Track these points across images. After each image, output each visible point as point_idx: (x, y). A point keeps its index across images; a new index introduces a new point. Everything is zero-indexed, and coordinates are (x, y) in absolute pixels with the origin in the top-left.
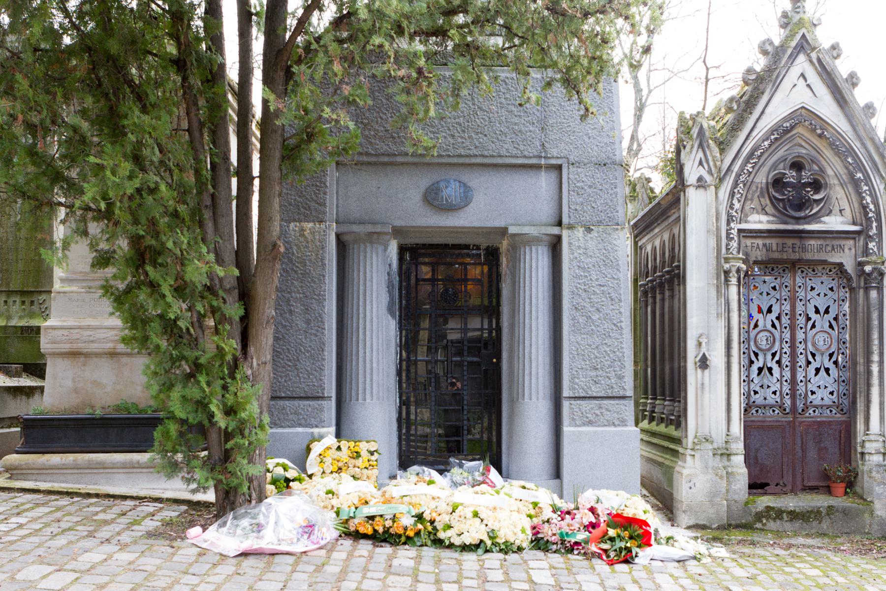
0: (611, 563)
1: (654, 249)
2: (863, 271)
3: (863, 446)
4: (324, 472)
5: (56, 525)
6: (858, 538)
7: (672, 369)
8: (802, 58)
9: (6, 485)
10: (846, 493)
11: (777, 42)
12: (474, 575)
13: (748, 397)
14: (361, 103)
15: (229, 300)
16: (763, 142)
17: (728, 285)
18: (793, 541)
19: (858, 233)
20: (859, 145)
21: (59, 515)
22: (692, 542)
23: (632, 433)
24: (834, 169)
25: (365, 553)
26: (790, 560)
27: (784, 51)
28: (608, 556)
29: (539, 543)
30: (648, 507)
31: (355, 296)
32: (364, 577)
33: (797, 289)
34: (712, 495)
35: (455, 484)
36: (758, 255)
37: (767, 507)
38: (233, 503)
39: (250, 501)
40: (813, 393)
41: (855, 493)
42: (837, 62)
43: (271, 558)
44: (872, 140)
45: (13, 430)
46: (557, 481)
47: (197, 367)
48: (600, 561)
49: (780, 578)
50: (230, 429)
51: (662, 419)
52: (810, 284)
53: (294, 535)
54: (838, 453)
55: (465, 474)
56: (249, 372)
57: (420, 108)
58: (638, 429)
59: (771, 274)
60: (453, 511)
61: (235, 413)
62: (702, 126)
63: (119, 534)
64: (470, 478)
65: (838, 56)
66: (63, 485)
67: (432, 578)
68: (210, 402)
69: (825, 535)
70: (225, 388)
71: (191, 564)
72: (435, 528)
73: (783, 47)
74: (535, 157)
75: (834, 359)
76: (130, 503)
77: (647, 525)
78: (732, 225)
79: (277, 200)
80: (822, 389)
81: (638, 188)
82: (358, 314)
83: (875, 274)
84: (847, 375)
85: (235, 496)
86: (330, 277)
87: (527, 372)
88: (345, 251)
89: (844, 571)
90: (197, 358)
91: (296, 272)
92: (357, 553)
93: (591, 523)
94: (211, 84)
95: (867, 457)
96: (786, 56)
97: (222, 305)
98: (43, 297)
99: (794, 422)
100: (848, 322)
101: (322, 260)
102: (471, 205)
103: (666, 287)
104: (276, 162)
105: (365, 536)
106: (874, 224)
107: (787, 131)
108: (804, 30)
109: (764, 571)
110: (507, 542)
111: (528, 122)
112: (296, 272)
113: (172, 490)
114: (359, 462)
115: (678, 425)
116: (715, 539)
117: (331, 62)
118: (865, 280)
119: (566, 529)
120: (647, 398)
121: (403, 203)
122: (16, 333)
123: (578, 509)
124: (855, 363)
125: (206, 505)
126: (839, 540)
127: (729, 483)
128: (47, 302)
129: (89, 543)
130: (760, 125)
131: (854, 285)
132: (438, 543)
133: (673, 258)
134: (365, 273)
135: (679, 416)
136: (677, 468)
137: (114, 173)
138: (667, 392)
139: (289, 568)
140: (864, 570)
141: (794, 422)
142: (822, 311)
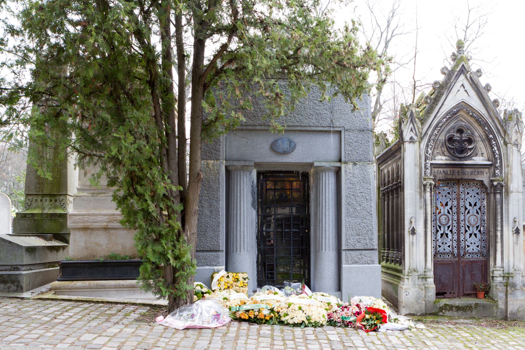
0: (367, 331)
1: (388, 172)
2: (493, 185)
3: (493, 273)
4: (220, 289)
5: (88, 316)
6: (490, 319)
7: (397, 235)
8: (462, 77)
9: (54, 298)
10: (485, 297)
11: (450, 69)
12: (301, 337)
13: (436, 249)
14: (249, 109)
15: (176, 202)
16: (443, 119)
17: (425, 192)
18: (458, 321)
19: (491, 165)
20: (491, 121)
21: (87, 311)
22: (407, 321)
23: (377, 268)
24: (478, 132)
25: (246, 328)
26: (455, 330)
27: (454, 73)
28: (366, 328)
29: (332, 323)
30: (386, 305)
31: (235, 198)
32: (247, 338)
33: (460, 194)
34: (418, 299)
35: (287, 295)
36: (441, 176)
37: (445, 304)
38: (178, 304)
39: (186, 303)
40: (468, 246)
41: (489, 297)
42: (480, 78)
43: (200, 330)
44: (497, 118)
45: (56, 268)
46: (339, 292)
47: (160, 236)
48: (361, 331)
49: (449, 337)
50: (177, 267)
51: (393, 260)
52: (467, 191)
53: (211, 319)
54: (481, 276)
55: (292, 290)
56: (186, 238)
57: (276, 110)
58: (380, 266)
59: (447, 186)
60: (289, 307)
61: (180, 259)
62: (412, 111)
63: (121, 320)
64: (295, 291)
65: (480, 75)
66: (83, 297)
67: (281, 339)
68: (167, 254)
69: (474, 318)
70: (174, 246)
71: (162, 333)
72: (279, 316)
73: (453, 71)
74: (327, 126)
75: (479, 229)
76: (120, 306)
77: (385, 312)
78: (427, 161)
79: (199, 151)
80: (473, 244)
81: (380, 139)
82: (237, 207)
83: (499, 186)
84: (485, 237)
85: (179, 301)
86: (223, 188)
87: (324, 237)
88: (229, 175)
89: (481, 334)
90: (160, 232)
91: (205, 186)
92: (241, 328)
93: (357, 312)
94: (166, 93)
95: (495, 278)
96: (455, 76)
97: (172, 205)
98: (62, 197)
99: (459, 261)
100: (486, 210)
101: (218, 180)
102: (295, 151)
103: (395, 192)
104: (199, 132)
105: (245, 320)
106: (499, 161)
107: (455, 114)
108: (463, 63)
109: (442, 335)
110: (315, 322)
111: (324, 109)
112: (205, 186)
113: (141, 299)
114: (238, 284)
115: (400, 264)
116: (419, 321)
117: (235, 89)
118: (494, 189)
119: (344, 315)
120: (385, 250)
121: (260, 151)
122: (47, 217)
123: (350, 305)
124: (489, 231)
125: (160, 307)
126: (481, 320)
127: (426, 292)
128: (64, 200)
129: (108, 324)
130: (441, 110)
131: (489, 192)
132: (281, 323)
133: (398, 177)
134: (240, 186)
135: (401, 259)
136: (400, 285)
137: (125, 142)
138: (395, 247)
139: (210, 335)
140: (491, 334)
141: (459, 261)
142: (473, 205)
